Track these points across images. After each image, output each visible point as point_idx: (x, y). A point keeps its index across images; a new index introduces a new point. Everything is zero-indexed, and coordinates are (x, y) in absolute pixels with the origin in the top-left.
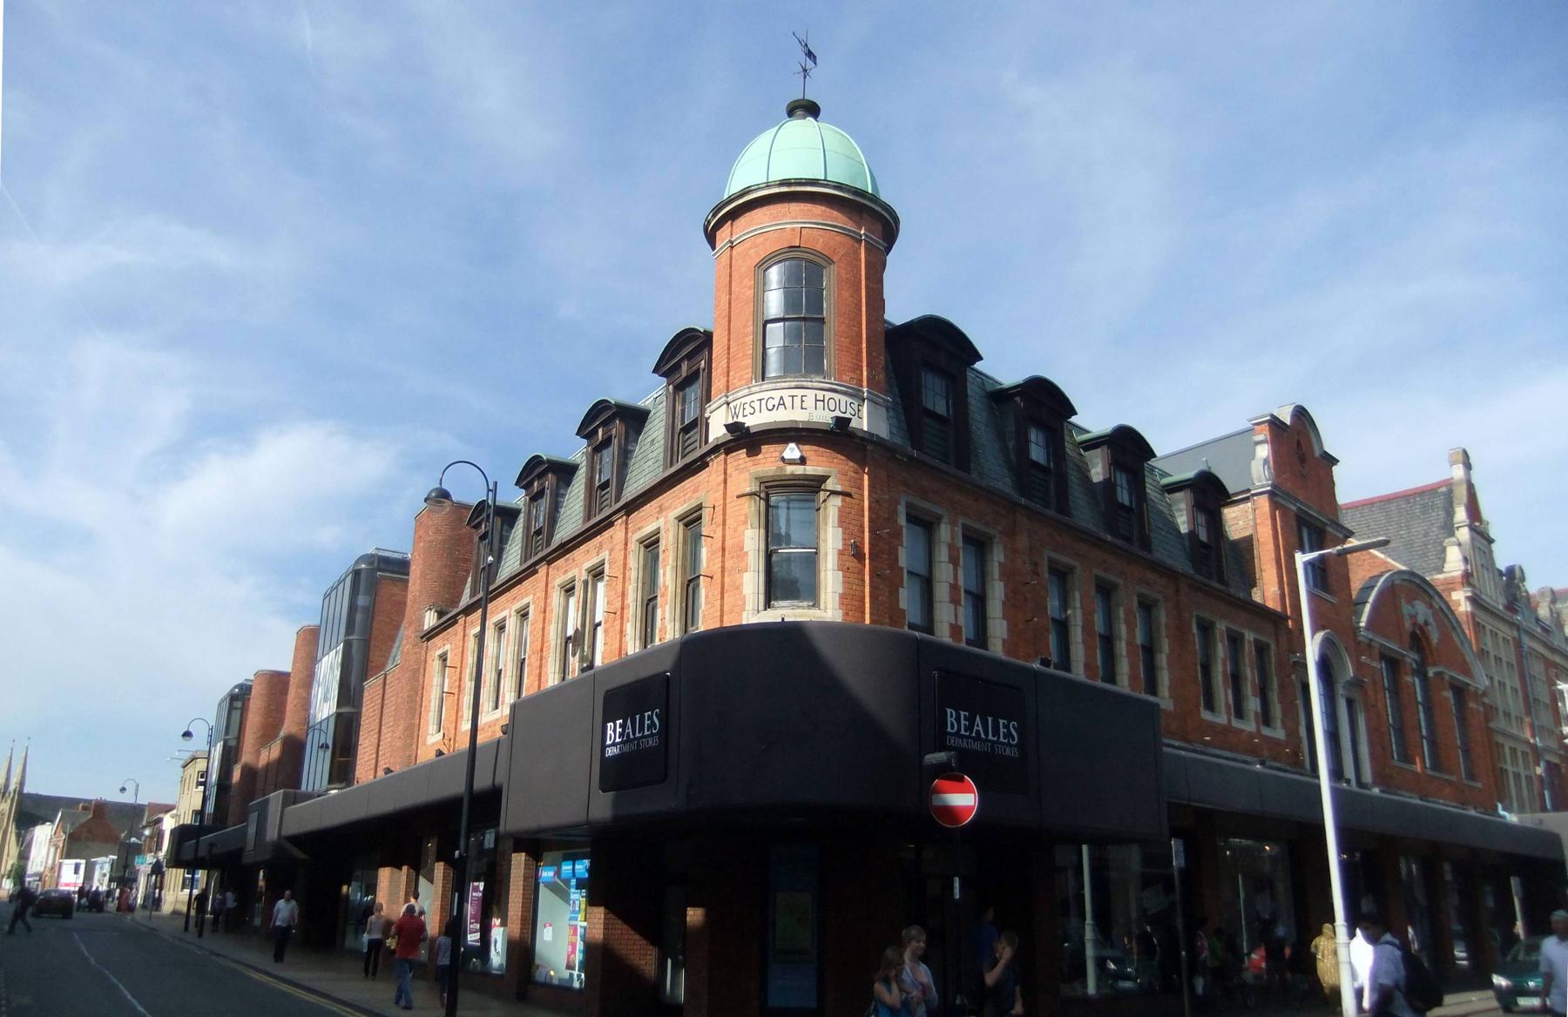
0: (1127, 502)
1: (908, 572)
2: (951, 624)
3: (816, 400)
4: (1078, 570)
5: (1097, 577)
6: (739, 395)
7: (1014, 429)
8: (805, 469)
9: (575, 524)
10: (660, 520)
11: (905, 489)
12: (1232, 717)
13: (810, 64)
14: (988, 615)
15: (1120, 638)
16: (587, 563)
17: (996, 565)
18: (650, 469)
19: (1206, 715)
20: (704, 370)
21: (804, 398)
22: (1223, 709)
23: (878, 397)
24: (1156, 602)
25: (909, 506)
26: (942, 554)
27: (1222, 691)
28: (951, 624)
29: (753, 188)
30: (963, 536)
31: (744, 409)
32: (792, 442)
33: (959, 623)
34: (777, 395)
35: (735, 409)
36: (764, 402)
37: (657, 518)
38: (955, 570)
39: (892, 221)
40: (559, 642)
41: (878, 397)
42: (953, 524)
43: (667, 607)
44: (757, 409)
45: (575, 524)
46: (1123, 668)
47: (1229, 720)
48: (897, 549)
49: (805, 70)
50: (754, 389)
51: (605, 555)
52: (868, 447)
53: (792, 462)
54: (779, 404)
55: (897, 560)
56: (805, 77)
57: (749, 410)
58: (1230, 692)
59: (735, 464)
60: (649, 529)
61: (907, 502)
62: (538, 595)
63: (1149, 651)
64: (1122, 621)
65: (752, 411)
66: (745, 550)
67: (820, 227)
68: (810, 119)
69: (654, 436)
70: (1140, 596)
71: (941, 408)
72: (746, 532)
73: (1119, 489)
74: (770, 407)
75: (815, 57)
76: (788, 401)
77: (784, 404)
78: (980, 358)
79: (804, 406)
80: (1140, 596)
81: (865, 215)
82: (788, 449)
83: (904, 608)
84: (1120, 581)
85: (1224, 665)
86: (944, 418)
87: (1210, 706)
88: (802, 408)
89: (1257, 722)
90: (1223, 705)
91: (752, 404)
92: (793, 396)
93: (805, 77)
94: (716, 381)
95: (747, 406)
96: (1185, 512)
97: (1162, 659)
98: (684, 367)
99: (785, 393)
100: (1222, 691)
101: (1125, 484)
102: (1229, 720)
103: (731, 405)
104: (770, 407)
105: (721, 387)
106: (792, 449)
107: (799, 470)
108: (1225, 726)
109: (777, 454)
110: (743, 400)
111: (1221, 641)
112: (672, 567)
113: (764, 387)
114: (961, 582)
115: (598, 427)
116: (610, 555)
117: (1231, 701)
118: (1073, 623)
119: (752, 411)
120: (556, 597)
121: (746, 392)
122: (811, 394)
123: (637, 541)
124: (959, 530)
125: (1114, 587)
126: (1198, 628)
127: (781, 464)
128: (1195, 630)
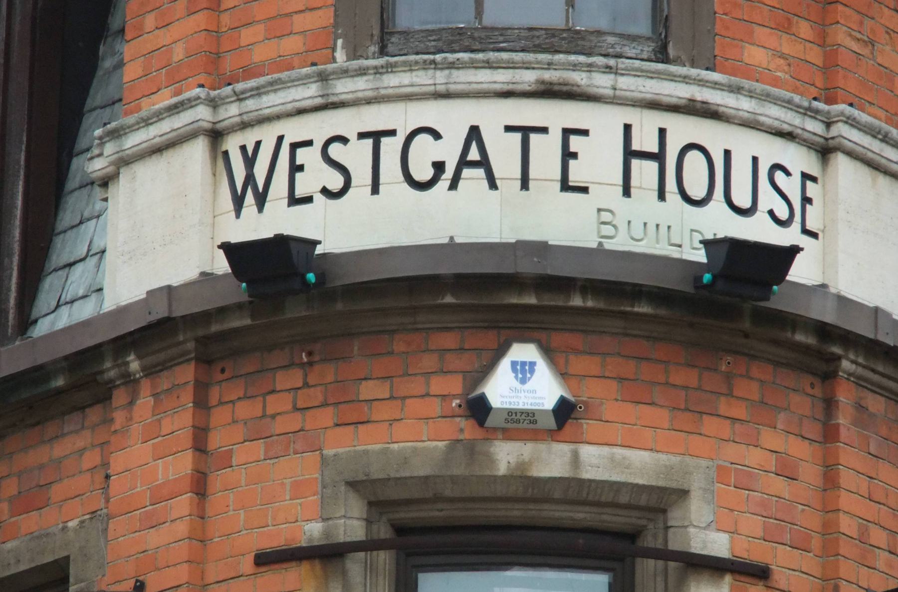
3: (630, 154)
6: (272, 102)
8: (575, 460)
21: (576, 143)
23: (631, 517)
31: (296, 168)
35: (250, 162)
36: (391, 148)
41: (631, 517)
44: (362, 174)
52: (845, 364)
54: (463, 163)
59: (245, 410)
65: (335, 181)
68: (124, 68)
77: (484, 163)
79: (575, 178)
82: (505, 365)
88: (566, 186)
91: (335, 151)
92: (526, 131)
95: (307, 157)
103: (232, 145)
104: (423, 173)
105: (179, 53)
106: (524, 370)
109: (454, 385)
110: (294, 130)
113: (394, 81)
119: (335, 181)
121: (308, 93)
127: (467, 428)
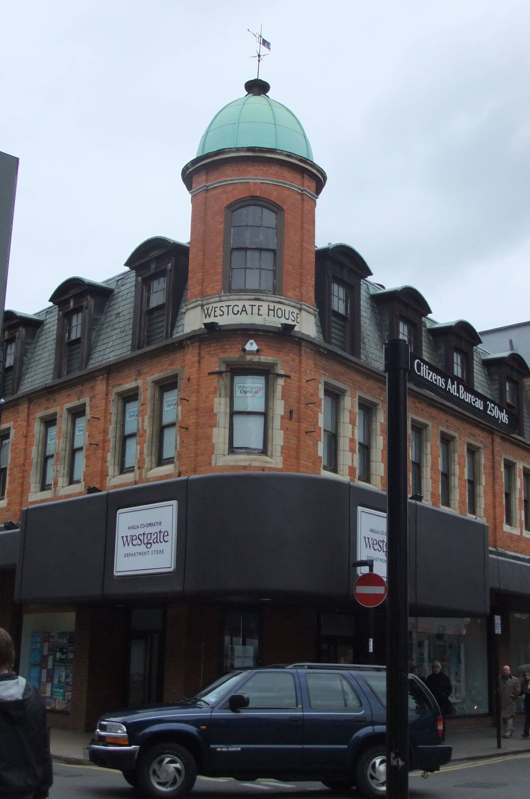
0: (460, 375)
1: (324, 430)
2: (349, 467)
3: (269, 310)
4: (430, 428)
5: (441, 431)
6: (211, 300)
7: (388, 323)
9: (43, 370)
10: (139, 381)
11: (324, 373)
12: (524, 530)
13: (264, 50)
14: (371, 459)
15: (454, 475)
16: (68, 404)
17: (378, 424)
18: (119, 336)
19: (506, 528)
20: (171, 271)
22: (518, 524)
24: (478, 448)
25: (326, 384)
26: (345, 417)
27: (518, 512)
28: (349, 467)
29: (227, 150)
30: (359, 404)
31: (215, 311)
32: (252, 339)
33: (354, 466)
34: (241, 304)
35: (208, 310)
36: (231, 308)
37: (136, 380)
38: (353, 428)
39: (322, 179)
40: (39, 460)
41: (310, 308)
42: (353, 397)
43: (145, 445)
44: (226, 312)
45: (43, 370)
46: (456, 495)
47: (521, 532)
48: (318, 415)
49: (259, 56)
50: (223, 298)
51: (86, 400)
53: (251, 353)
54: (242, 311)
55: (317, 422)
56: (259, 61)
57: (218, 312)
58: (523, 512)
60: (129, 385)
61: (325, 382)
62: (19, 423)
63: (472, 483)
64: (456, 463)
66: (215, 412)
67: (274, 183)
69: (120, 310)
70: (469, 445)
71: (341, 310)
72: (215, 399)
73: (455, 365)
74: (236, 312)
75: (269, 44)
76: (249, 309)
77: (245, 311)
78: (371, 274)
80: (469, 445)
81: (306, 176)
82: (249, 343)
83: (320, 455)
84: (456, 434)
85: (520, 493)
86: (343, 315)
87: (509, 521)
88: (259, 315)
89: (521, 527)
90: (518, 521)
91: (222, 308)
92: (252, 306)
93: (259, 61)
94: (192, 287)
96: (497, 382)
97: (481, 489)
98: (153, 266)
99: (247, 303)
100: (518, 512)
101: (459, 363)
102: (521, 532)
104: (236, 312)
106: (251, 344)
107: (256, 359)
108: (518, 536)
110: (215, 305)
111: (519, 477)
112: (150, 417)
114: (356, 437)
115: (70, 298)
116: (91, 401)
117: (523, 519)
118: (425, 464)
119: (222, 313)
120: (37, 428)
121: (217, 299)
122: (265, 305)
123: (116, 393)
124: (356, 400)
125: (453, 438)
126: (505, 468)
127: (243, 353)
128: (503, 469)
